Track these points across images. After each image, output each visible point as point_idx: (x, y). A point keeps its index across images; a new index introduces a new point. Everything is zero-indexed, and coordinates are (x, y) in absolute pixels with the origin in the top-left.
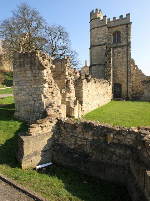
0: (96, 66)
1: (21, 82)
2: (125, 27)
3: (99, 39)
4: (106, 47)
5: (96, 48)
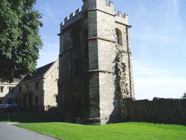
2: (125, 27)
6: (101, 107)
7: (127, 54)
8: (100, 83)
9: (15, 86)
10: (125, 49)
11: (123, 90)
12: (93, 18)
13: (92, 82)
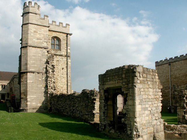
0: (34, 74)
1: (144, 100)
3: (38, 39)
4: (48, 52)
5: (34, 49)
6: (28, 100)
7: (65, 57)
8: (28, 81)
9: (6, 84)
10: (64, 53)
11: (50, 86)
12: (26, 30)
13: (22, 80)
